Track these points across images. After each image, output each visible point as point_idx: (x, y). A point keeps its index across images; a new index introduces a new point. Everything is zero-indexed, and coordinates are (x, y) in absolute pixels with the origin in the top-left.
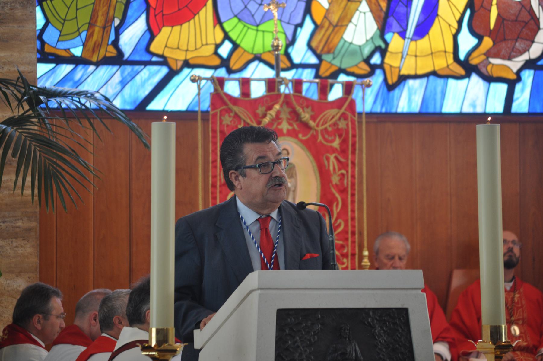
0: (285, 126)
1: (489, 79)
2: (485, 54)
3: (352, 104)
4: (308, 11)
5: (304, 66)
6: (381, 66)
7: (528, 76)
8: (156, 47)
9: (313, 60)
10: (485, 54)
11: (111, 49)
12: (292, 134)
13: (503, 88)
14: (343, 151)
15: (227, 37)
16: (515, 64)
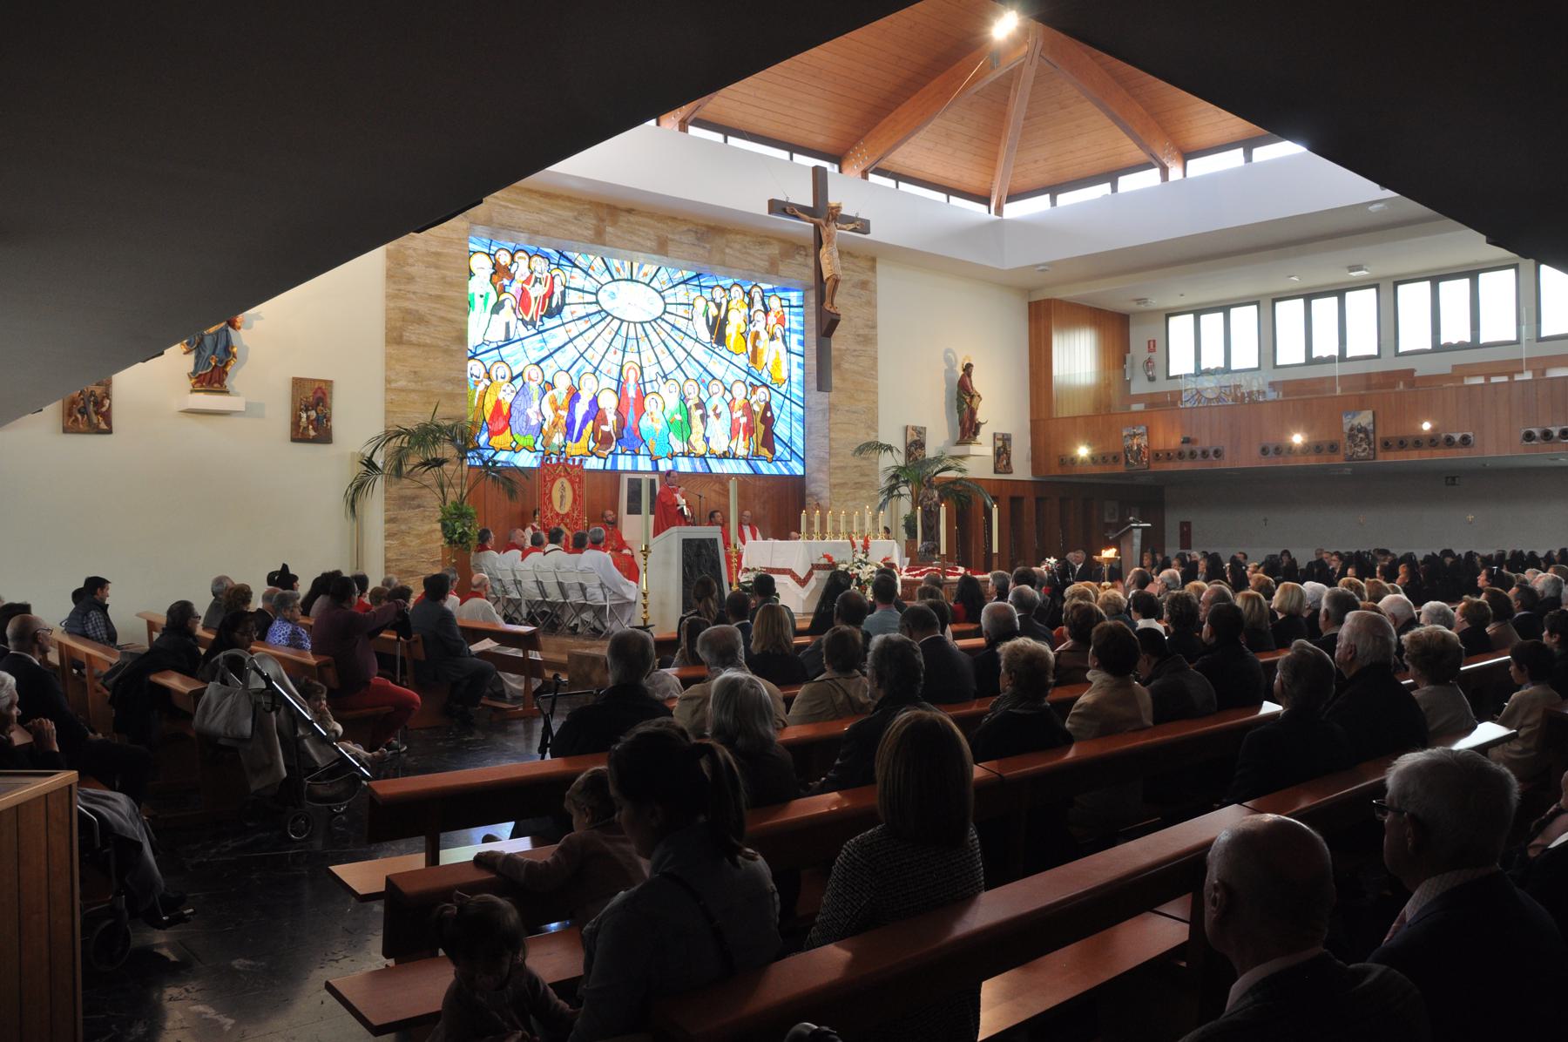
0: (563, 474)
1: (598, 457)
2: (1129, 381)
3: (582, 467)
4: (541, 432)
5: (539, 451)
6: (564, 452)
7: (611, 456)
8: (491, 443)
9: (543, 449)
10: (1129, 381)
11: (657, 286)
12: (565, 476)
13: (603, 461)
14: (580, 483)
15: (514, 440)
16: (607, 452)
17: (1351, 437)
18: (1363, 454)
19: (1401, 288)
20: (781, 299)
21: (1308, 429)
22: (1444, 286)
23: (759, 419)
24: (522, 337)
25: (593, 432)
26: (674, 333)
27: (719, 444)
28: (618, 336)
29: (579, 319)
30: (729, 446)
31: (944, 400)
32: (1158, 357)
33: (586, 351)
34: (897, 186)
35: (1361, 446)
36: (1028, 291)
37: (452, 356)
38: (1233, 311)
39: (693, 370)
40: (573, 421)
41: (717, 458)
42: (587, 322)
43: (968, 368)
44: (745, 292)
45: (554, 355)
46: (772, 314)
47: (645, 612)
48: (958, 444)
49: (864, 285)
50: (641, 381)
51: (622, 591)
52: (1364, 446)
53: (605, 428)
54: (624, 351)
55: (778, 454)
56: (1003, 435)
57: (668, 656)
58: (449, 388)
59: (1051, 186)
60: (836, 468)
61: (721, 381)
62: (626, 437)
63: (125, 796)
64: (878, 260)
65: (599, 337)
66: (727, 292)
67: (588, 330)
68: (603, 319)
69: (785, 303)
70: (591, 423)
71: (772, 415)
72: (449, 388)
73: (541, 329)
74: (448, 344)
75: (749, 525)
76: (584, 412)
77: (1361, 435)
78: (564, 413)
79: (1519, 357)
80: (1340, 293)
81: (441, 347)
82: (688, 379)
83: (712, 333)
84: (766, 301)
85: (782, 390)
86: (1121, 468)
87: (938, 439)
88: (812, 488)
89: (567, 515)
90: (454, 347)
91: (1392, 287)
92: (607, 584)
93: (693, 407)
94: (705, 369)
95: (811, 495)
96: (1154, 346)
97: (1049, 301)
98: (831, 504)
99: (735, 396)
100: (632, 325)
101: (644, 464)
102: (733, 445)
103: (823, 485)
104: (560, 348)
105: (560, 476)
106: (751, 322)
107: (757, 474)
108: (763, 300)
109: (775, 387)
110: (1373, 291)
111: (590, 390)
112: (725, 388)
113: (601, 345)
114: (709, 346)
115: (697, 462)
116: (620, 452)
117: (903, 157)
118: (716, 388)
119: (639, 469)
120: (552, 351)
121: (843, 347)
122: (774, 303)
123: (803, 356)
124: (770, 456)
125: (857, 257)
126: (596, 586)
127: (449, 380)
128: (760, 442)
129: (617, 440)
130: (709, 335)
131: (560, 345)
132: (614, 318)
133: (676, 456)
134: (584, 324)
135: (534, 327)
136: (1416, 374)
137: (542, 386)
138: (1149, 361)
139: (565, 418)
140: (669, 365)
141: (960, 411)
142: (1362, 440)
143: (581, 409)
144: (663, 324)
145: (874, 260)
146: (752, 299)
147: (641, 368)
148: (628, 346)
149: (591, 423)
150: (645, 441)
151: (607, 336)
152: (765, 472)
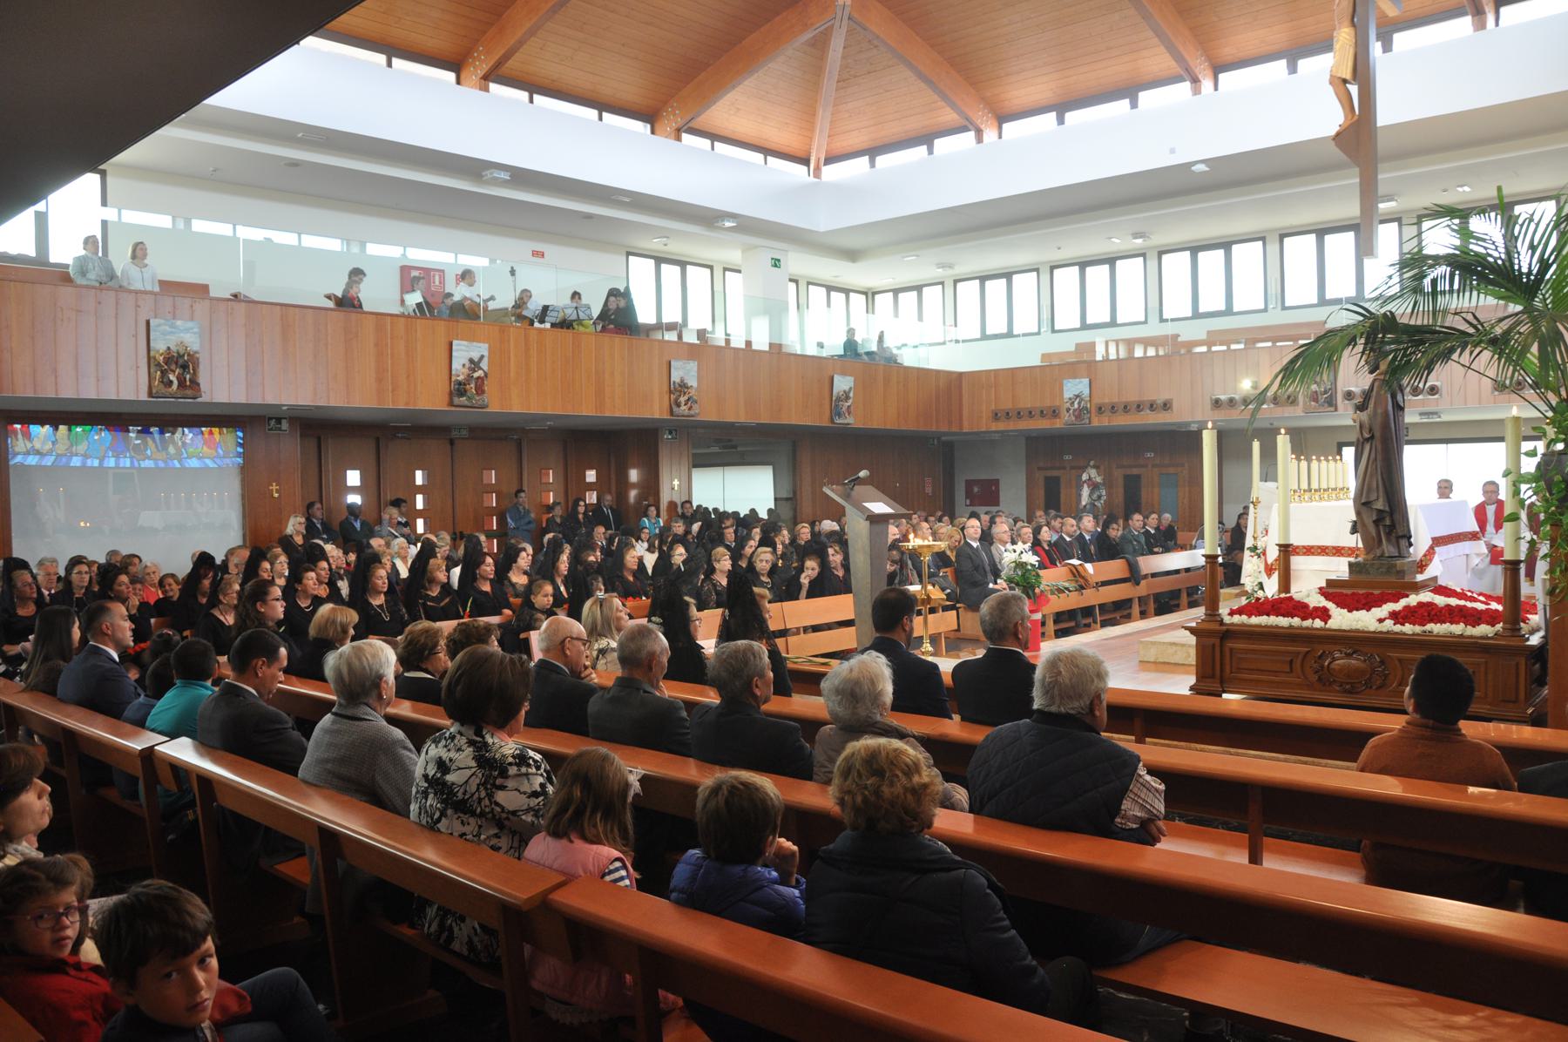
22: (1330, 239)
34: (713, 148)
38: (925, 289)
57: (1522, 904)
59: (870, 149)
80: (1226, 245)
91: (1156, 257)
110: (1261, 243)
117: (722, 113)
136: (1180, 339)
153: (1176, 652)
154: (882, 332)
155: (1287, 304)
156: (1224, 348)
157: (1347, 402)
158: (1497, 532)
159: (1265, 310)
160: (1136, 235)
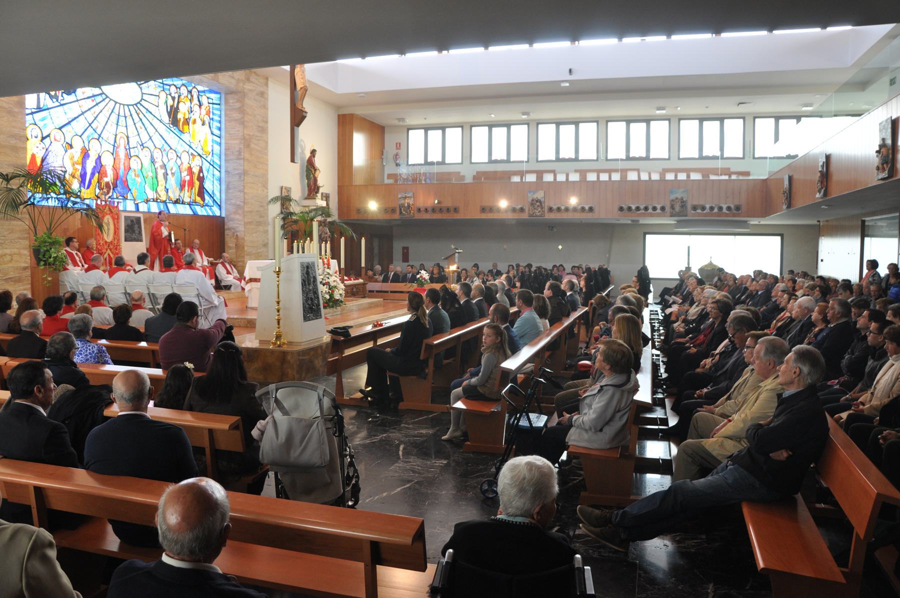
12: (109, 214)
17: (532, 204)
18: (539, 214)
19: (609, 124)
20: (208, 98)
21: (509, 198)
23: (196, 178)
24: (49, 107)
25: (98, 182)
26: (148, 115)
27: (174, 194)
28: (113, 113)
29: (88, 98)
30: (180, 196)
31: (299, 171)
32: (402, 152)
33: (93, 122)
35: (537, 209)
36: (337, 107)
37: (15, 116)
39: (159, 142)
40: (85, 174)
41: (173, 203)
42: (93, 101)
43: (313, 152)
44: (188, 91)
45: (71, 123)
46: (203, 107)
47: (279, 315)
48: (306, 199)
49: (262, 94)
50: (127, 147)
51: (212, 298)
52: (539, 209)
53: (106, 180)
54: (117, 124)
55: (206, 202)
56: (326, 194)
58: (13, 142)
60: (247, 212)
61: (175, 151)
62: (120, 184)
63: (656, 538)
64: (269, 79)
65: (82, 116)
66: (178, 89)
67: (93, 107)
68: (104, 100)
69: (210, 101)
70: (97, 175)
71: (203, 176)
72: (13, 142)
73: (62, 102)
74: (11, 106)
75: (198, 249)
76: (92, 167)
77: (538, 204)
78: (79, 167)
79: (717, 167)
81: (5, 108)
82: (156, 148)
83: (170, 117)
84: (200, 98)
85: (208, 159)
86: (397, 216)
87: (297, 193)
88: (229, 224)
89: (111, 242)
90: (16, 110)
92: (203, 295)
93: (159, 168)
94: (166, 142)
95: (229, 229)
96: (400, 146)
97: (352, 115)
98: (245, 235)
99: (183, 162)
100: (122, 106)
101: (130, 206)
102: (182, 195)
103: (239, 223)
104: (75, 118)
105: (107, 214)
106: (191, 112)
107: (195, 214)
108: (198, 97)
109: (204, 156)
111: (96, 151)
112: (177, 156)
113: (102, 119)
114: (168, 125)
115: (162, 205)
116: (115, 197)
118: (172, 155)
119: (127, 209)
120: (70, 120)
121: (251, 134)
122: (204, 100)
123: (220, 137)
124: (202, 203)
125: (259, 76)
126: (194, 295)
127: (13, 136)
128: (196, 193)
129: (113, 189)
130: (168, 118)
131: (76, 116)
132: (111, 100)
133: (150, 201)
134: (91, 102)
135: (57, 101)
137: (64, 146)
138: (397, 155)
139: (80, 171)
140: (145, 138)
141: (308, 177)
142: (538, 206)
143: (90, 164)
144: (141, 108)
145: (267, 79)
146: (192, 96)
147: (128, 137)
148: (120, 121)
149: (97, 175)
150: (130, 190)
151: (106, 113)
152: (200, 213)
153: (816, 339)
154: (775, 142)
155: (742, 156)
156: (726, 177)
157: (619, 212)
158: (231, 285)
159: (669, 159)
160: (524, 114)
